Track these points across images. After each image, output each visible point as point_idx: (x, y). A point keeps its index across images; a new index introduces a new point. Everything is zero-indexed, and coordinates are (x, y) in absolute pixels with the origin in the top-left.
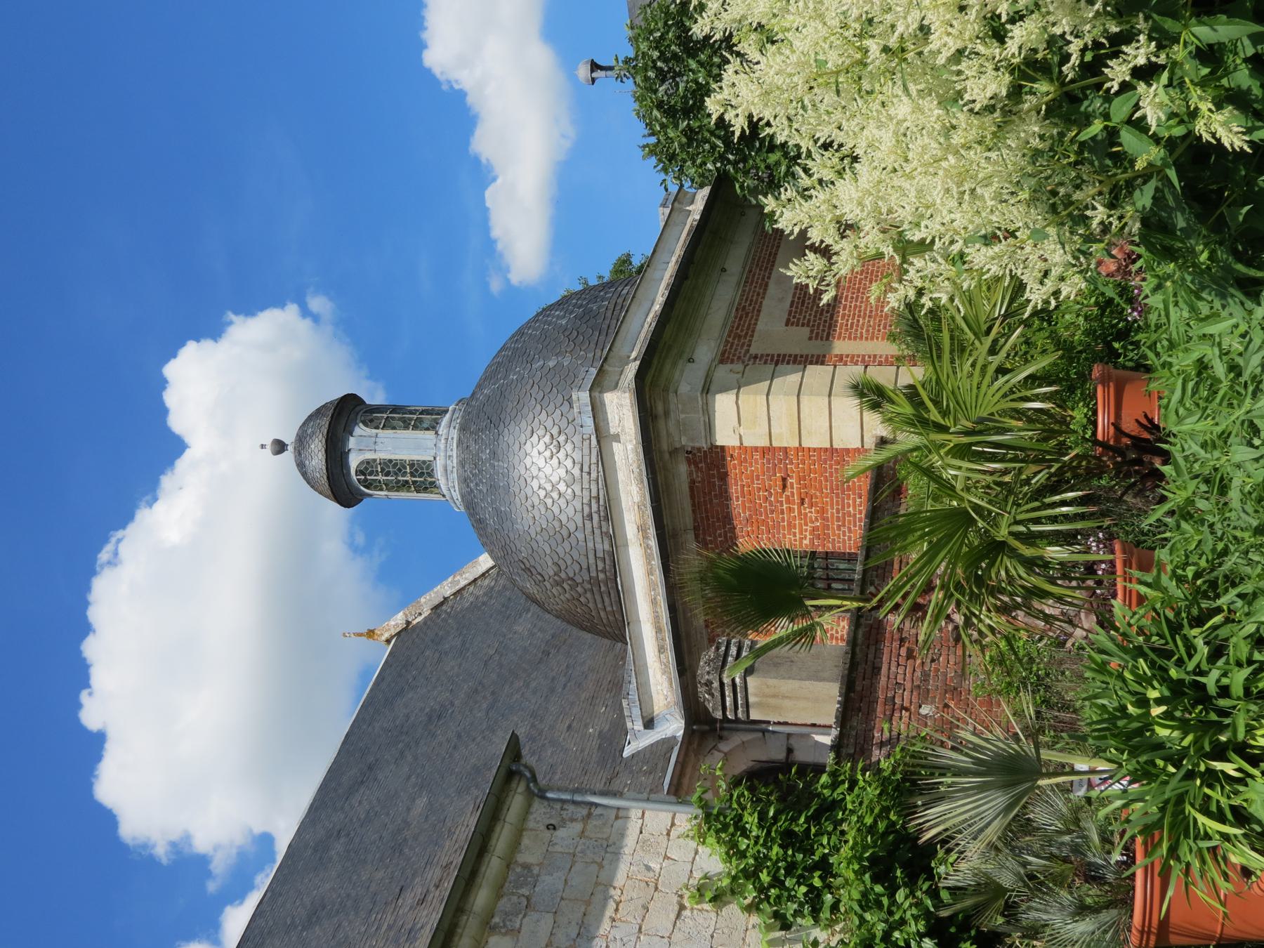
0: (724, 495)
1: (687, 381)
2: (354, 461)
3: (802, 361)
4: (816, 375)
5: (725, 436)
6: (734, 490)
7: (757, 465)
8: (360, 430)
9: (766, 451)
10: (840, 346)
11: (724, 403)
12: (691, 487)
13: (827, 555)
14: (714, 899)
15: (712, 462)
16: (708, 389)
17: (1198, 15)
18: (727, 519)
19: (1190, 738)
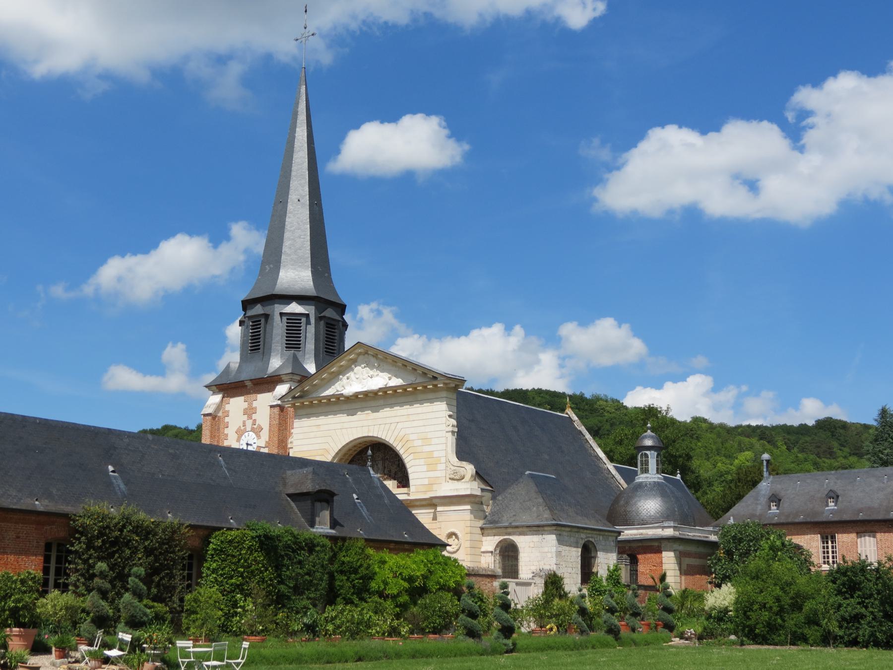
0: (651, 553)
1: (676, 546)
2: (648, 452)
3: (680, 569)
4: (678, 573)
5: (664, 554)
6: (652, 555)
7: (658, 561)
8: (656, 454)
9: (661, 563)
10: (683, 577)
11: (672, 554)
12: (654, 546)
13: (637, 575)
14: (281, 408)
15: (659, 551)
16: (674, 551)
17: (126, 628)
18: (645, 553)
19: (145, 646)
